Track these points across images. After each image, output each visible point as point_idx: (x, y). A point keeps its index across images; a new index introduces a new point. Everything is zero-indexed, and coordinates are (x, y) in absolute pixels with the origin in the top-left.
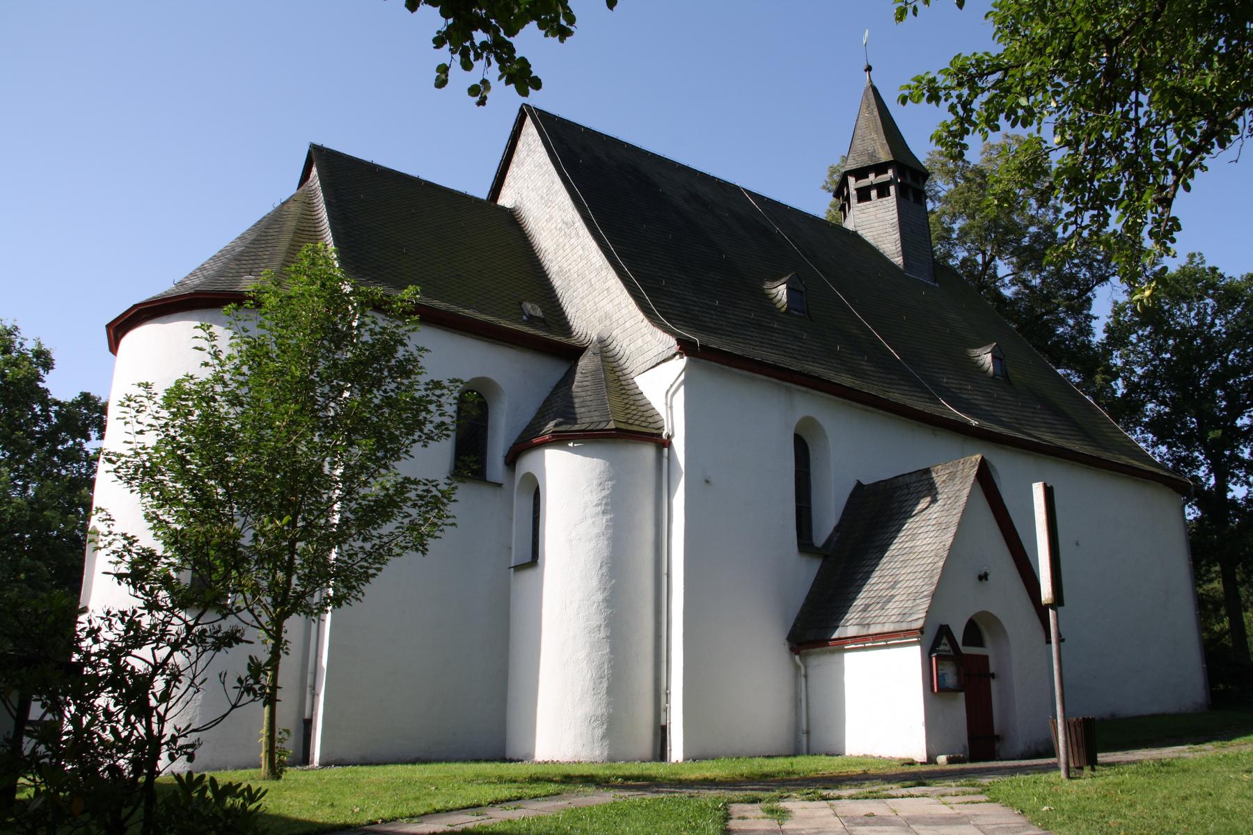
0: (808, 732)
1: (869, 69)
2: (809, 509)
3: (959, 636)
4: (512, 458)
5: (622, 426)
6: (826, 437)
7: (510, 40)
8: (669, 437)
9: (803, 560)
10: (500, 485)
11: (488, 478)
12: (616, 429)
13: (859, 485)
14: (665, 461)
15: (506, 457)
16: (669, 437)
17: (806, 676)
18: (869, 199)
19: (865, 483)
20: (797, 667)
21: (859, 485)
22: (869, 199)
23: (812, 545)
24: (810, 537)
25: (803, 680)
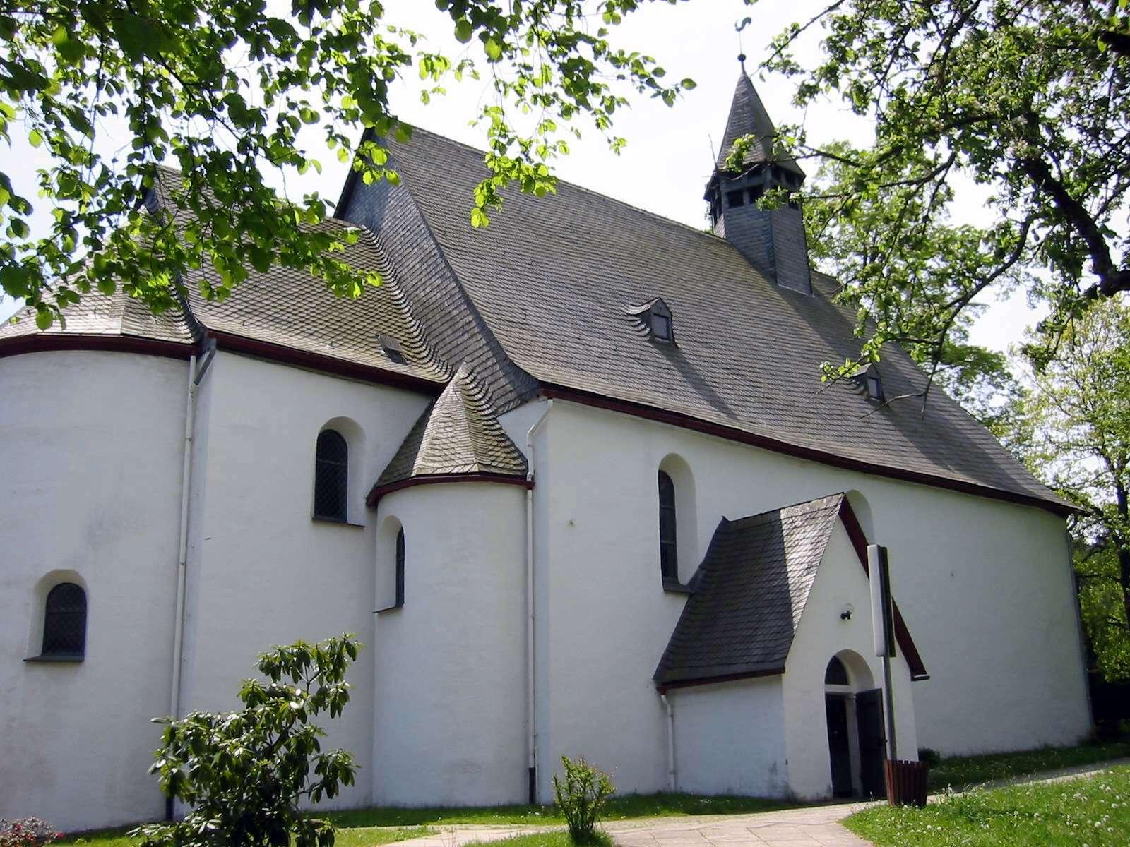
0: (675, 772)
1: (742, 58)
2: (674, 547)
3: (390, 55)
4: (374, 500)
5: (484, 469)
6: (690, 473)
7: (358, 107)
8: (533, 478)
9: (670, 598)
10: (361, 527)
11: (350, 520)
12: (480, 472)
13: (725, 521)
14: (530, 503)
15: (368, 499)
16: (533, 478)
17: (672, 716)
18: (741, 203)
19: (399, 119)
20: (663, 707)
21: (725, 521)
22: (741, 203)
23: (678, 582)
24: (676, 575)
25: (670, 719)
